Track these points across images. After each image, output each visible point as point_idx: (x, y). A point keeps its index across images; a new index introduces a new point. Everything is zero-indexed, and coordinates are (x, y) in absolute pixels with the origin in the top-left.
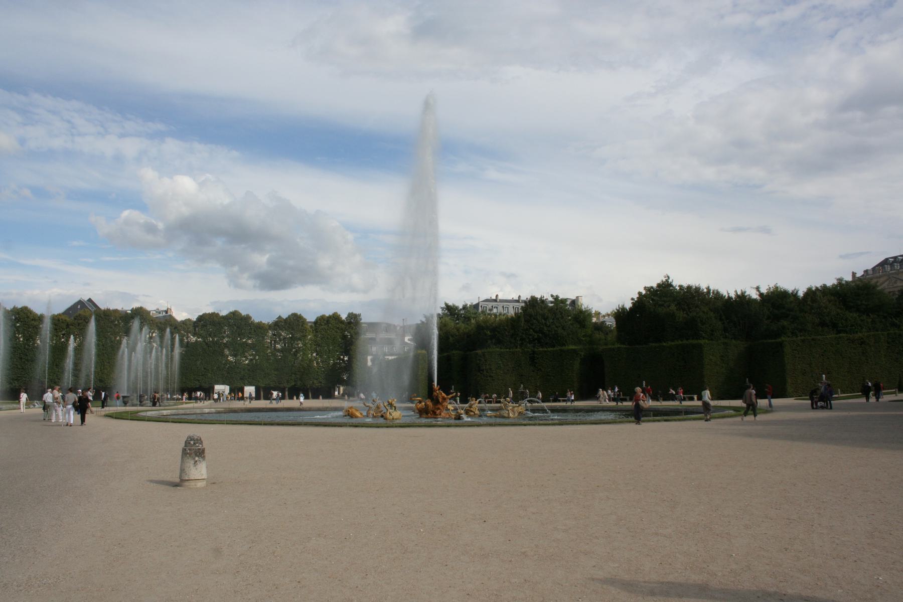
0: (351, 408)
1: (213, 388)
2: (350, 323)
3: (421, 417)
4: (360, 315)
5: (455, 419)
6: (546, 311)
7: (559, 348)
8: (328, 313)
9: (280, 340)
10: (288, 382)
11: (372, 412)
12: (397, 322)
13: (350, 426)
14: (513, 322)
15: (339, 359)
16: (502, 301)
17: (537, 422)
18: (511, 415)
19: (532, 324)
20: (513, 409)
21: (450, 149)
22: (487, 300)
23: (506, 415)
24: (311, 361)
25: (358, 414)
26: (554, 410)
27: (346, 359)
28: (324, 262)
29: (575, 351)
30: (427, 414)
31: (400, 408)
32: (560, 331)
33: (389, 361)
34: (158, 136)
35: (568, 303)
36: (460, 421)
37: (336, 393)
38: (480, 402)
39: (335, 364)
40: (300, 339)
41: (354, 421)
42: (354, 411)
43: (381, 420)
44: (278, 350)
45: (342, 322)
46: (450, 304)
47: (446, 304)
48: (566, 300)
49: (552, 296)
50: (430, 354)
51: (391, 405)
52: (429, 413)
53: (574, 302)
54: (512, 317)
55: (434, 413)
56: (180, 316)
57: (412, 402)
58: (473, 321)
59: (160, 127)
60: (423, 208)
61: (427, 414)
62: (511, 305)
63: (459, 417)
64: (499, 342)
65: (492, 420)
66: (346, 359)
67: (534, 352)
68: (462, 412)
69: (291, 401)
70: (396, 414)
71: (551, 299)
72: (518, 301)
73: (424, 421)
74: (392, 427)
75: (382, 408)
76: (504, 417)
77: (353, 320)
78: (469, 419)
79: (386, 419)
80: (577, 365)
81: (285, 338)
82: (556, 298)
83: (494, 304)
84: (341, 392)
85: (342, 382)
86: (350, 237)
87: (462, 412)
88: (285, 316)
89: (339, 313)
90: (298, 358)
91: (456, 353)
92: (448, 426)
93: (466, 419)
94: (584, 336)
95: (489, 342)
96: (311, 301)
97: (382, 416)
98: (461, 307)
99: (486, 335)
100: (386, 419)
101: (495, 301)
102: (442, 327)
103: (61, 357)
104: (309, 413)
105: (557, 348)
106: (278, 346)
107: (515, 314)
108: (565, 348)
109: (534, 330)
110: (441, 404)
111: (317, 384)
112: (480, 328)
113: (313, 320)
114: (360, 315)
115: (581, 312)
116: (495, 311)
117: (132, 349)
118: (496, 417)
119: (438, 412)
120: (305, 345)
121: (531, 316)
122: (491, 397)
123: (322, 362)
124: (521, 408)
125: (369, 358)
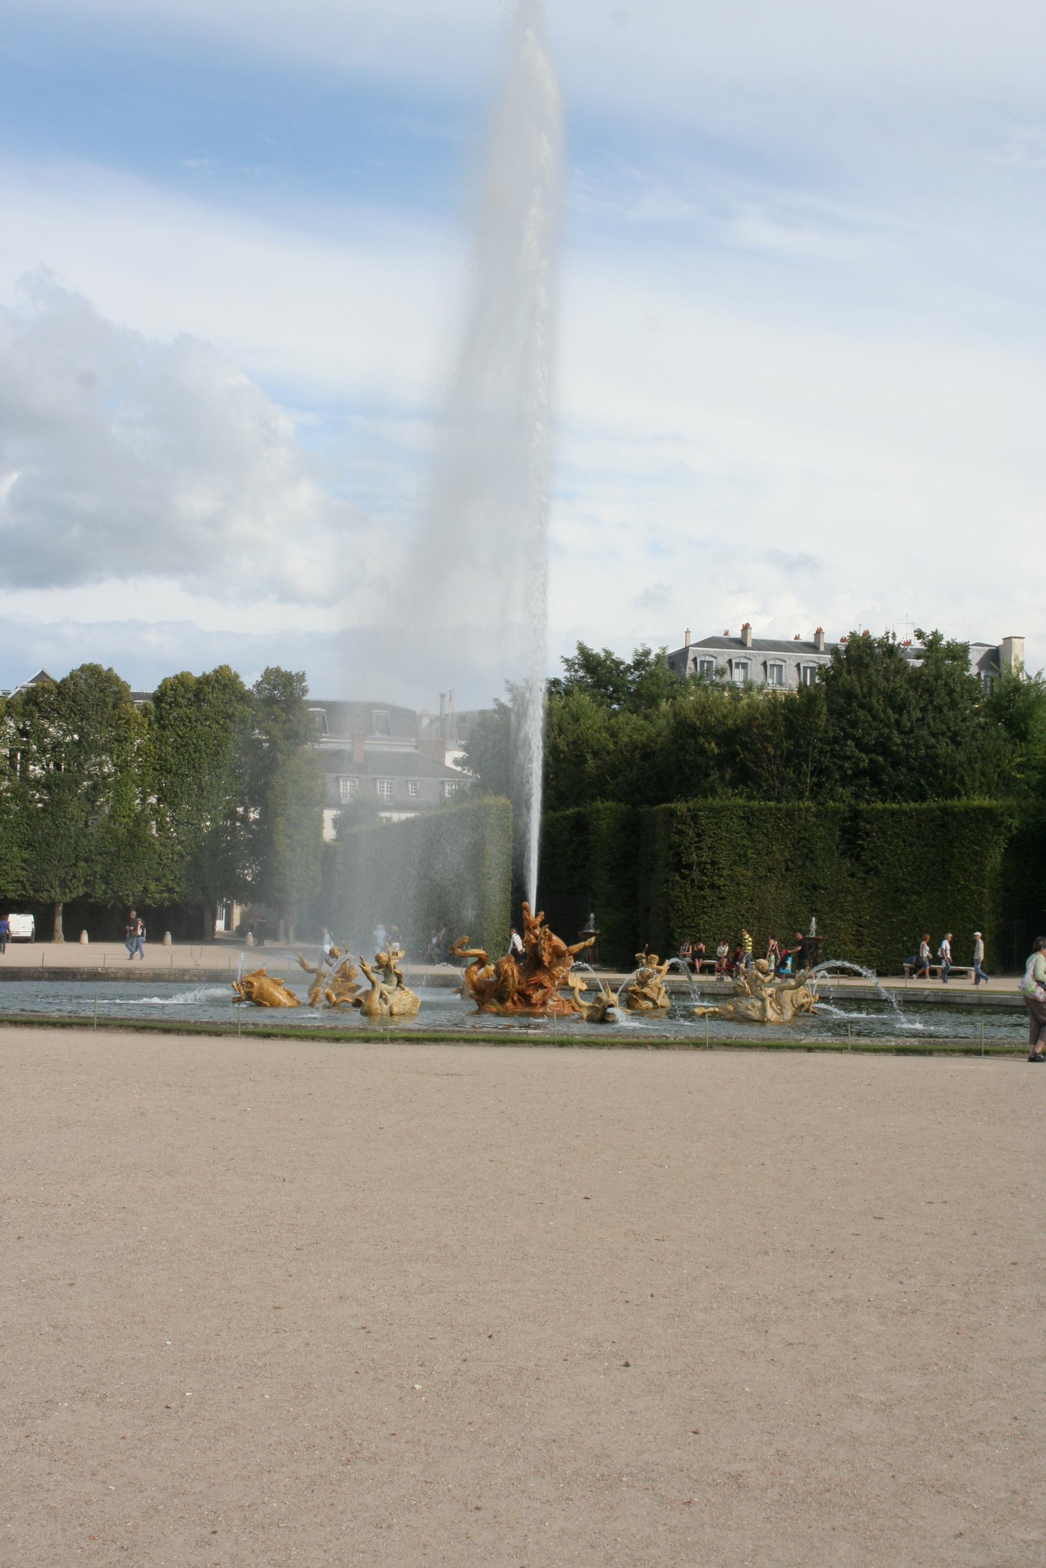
0: (259, 974)
2: (271, 701)
3: (480, 1011)
4: (301, 677)
5: (591, 1020)
6: (900, 681)
7: (942, 802)
8: (200, 666)
9: (43, 750)
10: (64, 884)
11: (324, 990)
12: (422, 702)
13: (248, 1034)
14: (794, 714)
15: (232, 815)
16: (761, 645)
17: (851, 1040)
18: (770, 1014)
19: (854, 725)
20: (782, 995)
21: (609, 142)
22: (712, 642)
23: (755, 1014)
24: (140, 820)
25: (280, 995)
26: (913, 1003)
27: (254, 815)
28: (195, 503)
29: (989, 813)
30: (502, 1000)
31: (415, 981)
32: (944, 747)
33: (391, 827)
35: (975, 656)
36: (603, 1029)
37: (220, 925)
38: (674, 969)
39: (216, 832)
40: (106, 749)
41: (262, 1017)
42: (267, 983)
43: (354, 1019)
44: (37, 783)
45: (244, 697)
46: (596, 649)
47: (582, 650)
48: (965, 648)
49: (920, 635)
50: (520, 805)
51: (385, 968)
52: (506, 998)
53: (994, 657)
54: (790, 699)
55: (525, 998)
56: (260, 679)
57: (454, 959)
58: (664, 706)
60: (503, 327)
61: (502, 1000)
62: (791, 659)
63: (601, 1016)
64: (745, 778)
65: (706, 1030)
66: (254, 815)
67: (856, 815)
68: (614, 997)
69: (73, 946)
70: (402, 999)
71: (917, 644)
72: (813, 647)
73: (490, 1023)
74: (381, 1040)
75: (360, 980)
76: (749, 1020)
77: (283, 689)
79: (367, 1013)
80: (995, 859)
81: (57, 745)
82: (933, 644)
83: (736, 654)
84: (236, 922)
85: (237, 891)
86: (285, 423)
87: (614, 997)
88: (59, 674)
89: (234, 669)
90: (95, 811)
91: (605, 810)
92: (562, 1044)
93: (623, 1019)
94: (1021, 767)
95: (715, 775)
96: (145, 628)
97: (358, 1003)
98: (629, 661)
99: (702, 751)
100: (367, 1013)
101: (741, 643)
102: (554, 728)
103: (59, 828)
104: (119, 987)
105: (932, 803)
106: (36, 770)
107: (802, 688)
108: (958, 803)
109: (860, 746)
110: (548, 970)
111: (157, 894)
112: (685, 730)
113: (151, 687)
114: (301, 677)
115: (1017, 688)
116: (738, 676)
118: (714, 1016)
119: (537, 996)
120: (122, 767)
121: (849, 696)
122: (712, 954)
123: (177, 823)
124: (805, 995)
125: (329, 815)
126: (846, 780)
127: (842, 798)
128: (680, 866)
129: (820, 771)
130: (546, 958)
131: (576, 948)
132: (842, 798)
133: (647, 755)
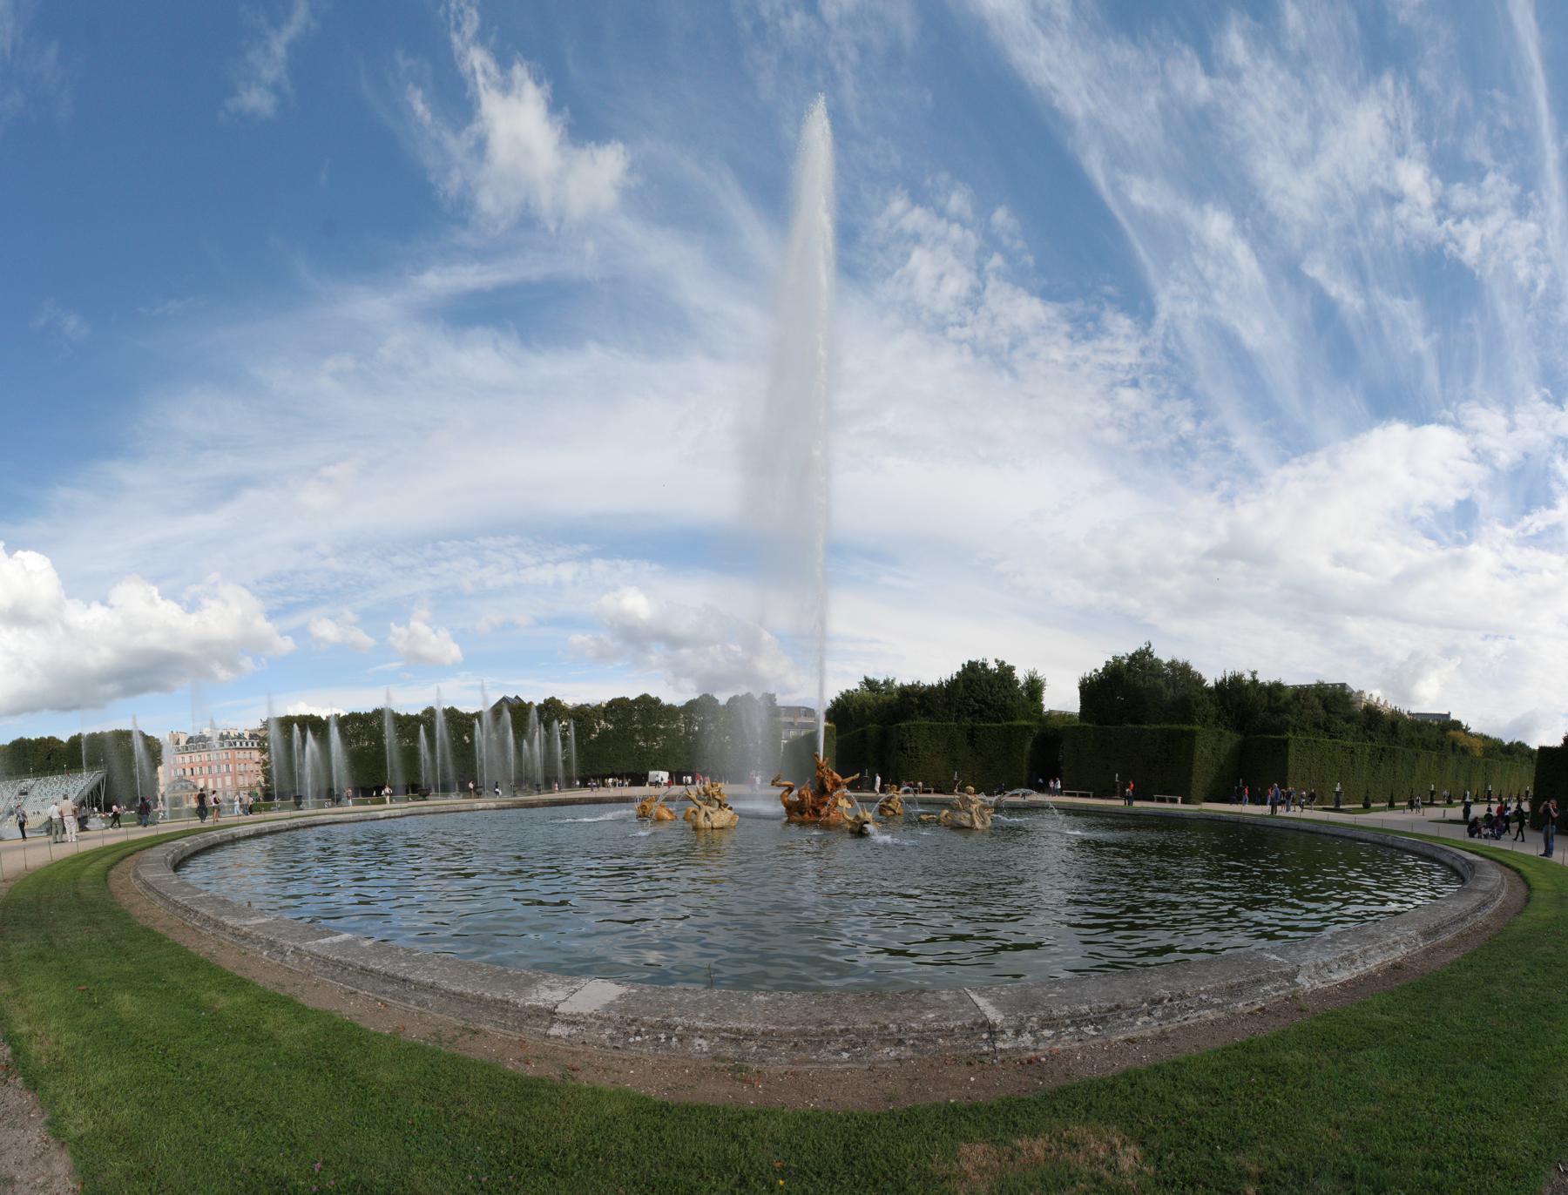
1: (647, 775)
18: (978, 825)
23: (966, 823)
29: (1027, 728)
34: (586, 558)
38: (906, 792)
46: (871, 677)
59: (584, 547)
64: (928, 713)
67: (973, 728)
78: (888, 838)
80: (1028, 747)
117: (531, 743)
121: (971, 681)
126: (970, 714)
127: (967, 722)
128: (903, 749)
129: (959, 711)
130: (829, 787)
131: (848, 780)
132: (967, 722)
133: (889, 706)
